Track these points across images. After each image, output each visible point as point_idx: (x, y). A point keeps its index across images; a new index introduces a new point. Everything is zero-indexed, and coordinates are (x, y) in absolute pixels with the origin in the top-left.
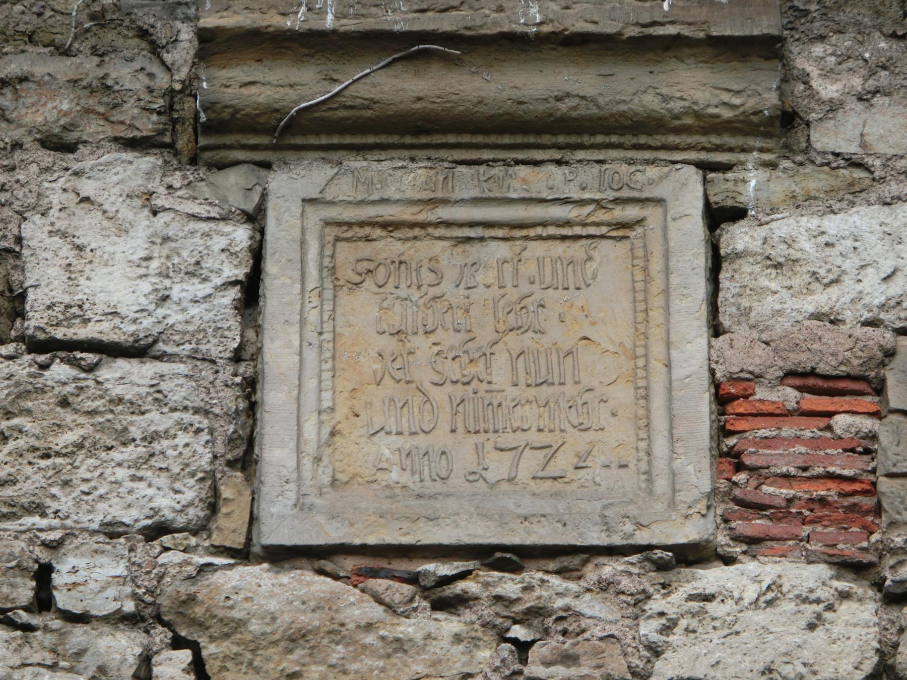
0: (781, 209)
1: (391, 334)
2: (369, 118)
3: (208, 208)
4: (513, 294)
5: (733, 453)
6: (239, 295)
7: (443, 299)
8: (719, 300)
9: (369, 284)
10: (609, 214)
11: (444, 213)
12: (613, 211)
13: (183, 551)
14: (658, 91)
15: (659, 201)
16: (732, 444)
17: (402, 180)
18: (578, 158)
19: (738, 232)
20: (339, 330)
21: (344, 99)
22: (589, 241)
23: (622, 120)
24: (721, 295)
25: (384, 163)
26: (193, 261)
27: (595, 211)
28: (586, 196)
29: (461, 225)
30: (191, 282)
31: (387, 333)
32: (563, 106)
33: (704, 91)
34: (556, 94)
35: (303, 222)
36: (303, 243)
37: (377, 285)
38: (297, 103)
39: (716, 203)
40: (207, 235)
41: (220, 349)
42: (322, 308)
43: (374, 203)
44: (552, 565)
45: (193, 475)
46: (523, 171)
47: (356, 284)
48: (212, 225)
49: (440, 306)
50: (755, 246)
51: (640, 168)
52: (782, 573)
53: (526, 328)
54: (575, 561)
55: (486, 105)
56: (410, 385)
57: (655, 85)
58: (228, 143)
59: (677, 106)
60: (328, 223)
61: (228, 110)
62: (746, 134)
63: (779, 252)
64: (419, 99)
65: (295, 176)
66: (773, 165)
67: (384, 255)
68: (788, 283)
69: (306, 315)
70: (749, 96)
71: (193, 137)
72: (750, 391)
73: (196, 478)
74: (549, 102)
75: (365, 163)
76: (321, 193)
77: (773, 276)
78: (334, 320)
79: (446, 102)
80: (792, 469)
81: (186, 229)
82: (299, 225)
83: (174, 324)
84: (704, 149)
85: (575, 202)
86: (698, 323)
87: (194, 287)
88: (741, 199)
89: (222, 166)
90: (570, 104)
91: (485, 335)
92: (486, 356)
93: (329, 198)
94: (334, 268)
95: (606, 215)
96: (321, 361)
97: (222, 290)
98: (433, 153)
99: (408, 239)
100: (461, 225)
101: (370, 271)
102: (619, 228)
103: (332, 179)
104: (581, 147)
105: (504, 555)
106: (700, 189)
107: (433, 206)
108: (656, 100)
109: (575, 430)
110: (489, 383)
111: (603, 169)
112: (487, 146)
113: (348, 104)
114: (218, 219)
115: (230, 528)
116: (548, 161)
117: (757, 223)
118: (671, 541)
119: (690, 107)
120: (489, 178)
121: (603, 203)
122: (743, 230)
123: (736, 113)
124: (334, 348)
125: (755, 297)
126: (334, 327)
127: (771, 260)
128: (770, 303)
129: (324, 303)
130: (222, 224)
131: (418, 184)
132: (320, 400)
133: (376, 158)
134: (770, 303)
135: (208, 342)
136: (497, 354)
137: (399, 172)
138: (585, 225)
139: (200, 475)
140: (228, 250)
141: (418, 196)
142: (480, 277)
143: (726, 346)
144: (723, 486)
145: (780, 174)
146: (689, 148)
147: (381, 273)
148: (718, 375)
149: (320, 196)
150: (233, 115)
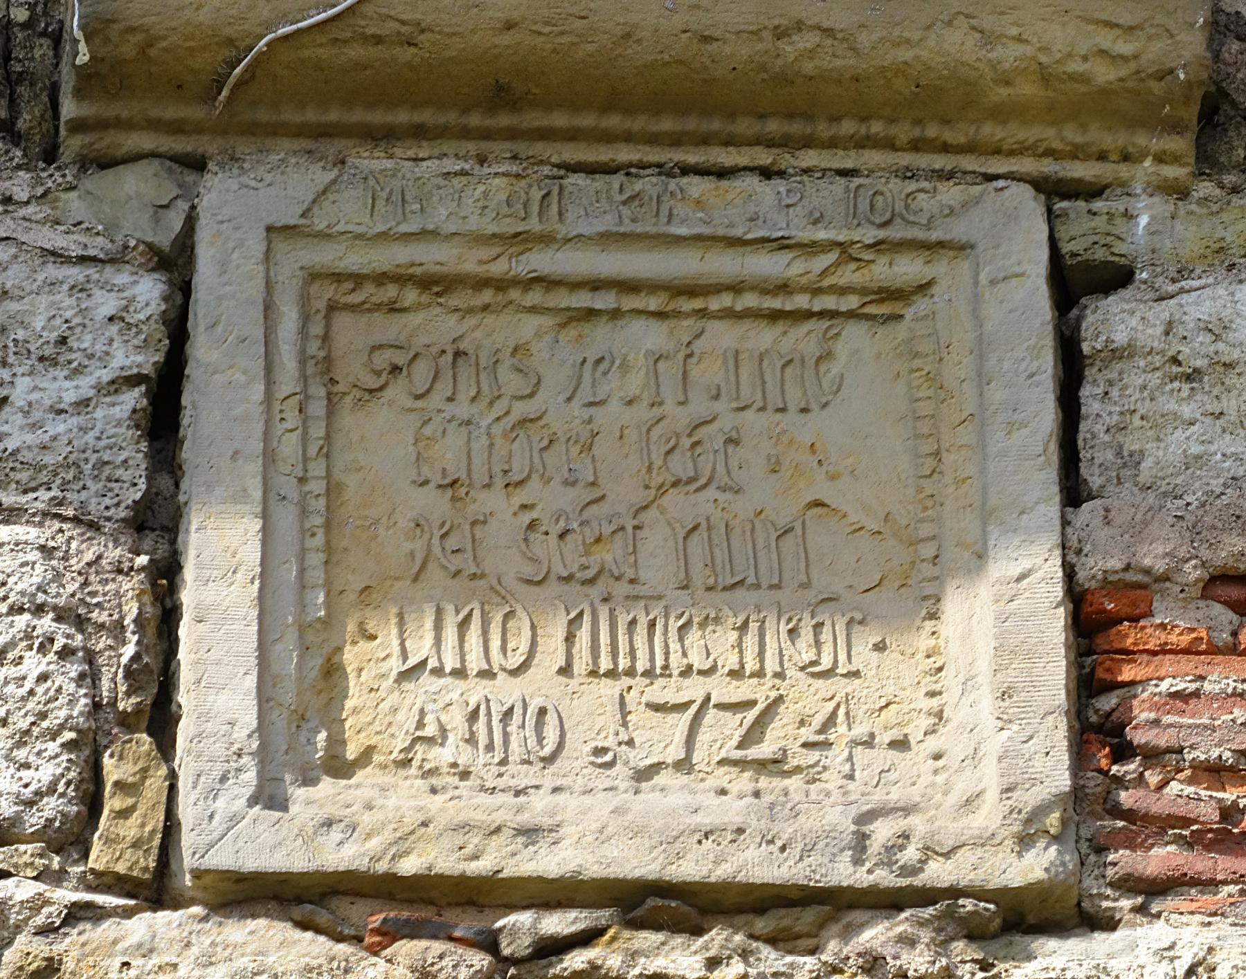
0: (1198, 271)
1: (440, 486)
2: (409, 65)
3: (82, 238)
4: (679, 418)
5: (1108, 725)
6: (145, 401)
7: (542, 423)
8: (1081, 437)
9: (397, 392)
10: (865, 271)
11: (540, 261)
12: (873, 267)
13: (35, 878)
14: (974, 22)
15: (963, 248)
16: (1107, 708)
17: (458, 201)
18: (804, 165)
19: (1115, 309)
20: (338, 475)
21: (363, 23)
22: (825, 324)
23: (899, 83)
24: (1083, 427)
25: (425, 164)
26: (54, 335)
27: (837, 264)
28: (822, 235)
29: (575, 285)
30: (50, 375)
31: (432, 485)
32: (788, 49)
33: (1064, 24)
34: (776, 22)
35: (268, 270)
36: (269, 308)
37: (410, 394)
38: (269, 27)
39: (1074, 255)
40: (79, 289)
41: (107, 501)
42: (305, 433)
43: (407, 237)
44: (762, 925)
45: (54, 734)
46: (697, 186)
47: (371, 391)
48: (92, 271)
49: (538, 437)
50: (1151, 336)
51: (925, 184)
52: (1216, 943)
53: (703, 481)
54: (809, 916)
55: (639, 41)
56: (476, 583)
57: (970, 10)
58: (124, 114)
59: (1008, 54)
60: (314, 275)
61: (139, 38)
62: (1134, 124)
63: (1196, 352)
64: (509, 26)
65: (253, 183)
66: (1180, 192)
67: (423, 340)
68: (1215, 407)
69: (275, 444)
70: (1150, 38)
71: (50, 113)
72: (1143, 608)
73: (59, 741)
74: (761, 40)
75: (389, 164)
76: (303, 215)
77: (1185, 394)
78: (327, 456)
79: (562, 33)
80: (1228, 754)
81: (41, 277)
82: (262, 275)
83: (18, 450)
84: (1050, 153)
85: (800, 245)
86: (1042, 476)
87: (56, 385)
88: (1120, 248)
89: (106, 163)
90: (801, 45)
91: (624, 492)
92: (631, 530)
93: (320, 225)
94: (328, 359)
95: (858, 274)
96: (303, 531)
97: (109, 394)
98: (523, 148)
99: (471, 311)
100: (575, 285)
101: (396, 369)
102: (882, 301)
103: (324, 192)
104: (809, 143)
105: (666, 902)
106: (1045, 228)
107: (521, 248)
108: (970, 42)
109: (801, 675)
110: (632, 581)
111: (853, 186)
112: (628, 138)
113: (371, 31)
114: (101, 261)
115: (117, 845)
116: (745, 169)
117: (1152, 295)
118: (995, 883)
119: (1033, 58)
120: (632, 198)
121: (853, 251)
122: (1126, 307)
123: (1123, 72)
124: (328, 508)
125: (1150, 433)
126: (328, 467)
127: (1180, 364)
128: (1179, 443)
129: (309, 424)
130: (109, 269)
131: (492, 204)
132: (302, 605)
133: (411, 153)
134: (1179, 443)
135: (84, 488)
136: (646, 529)
137: (455, 181)
138: (817, 291)
139: (69, 735)
140: (122, 319)
141: (492, 228)
142: (612, 385)
143: (1097, 521)
144: (1092, 784)
145: (1194, 207)
146: (1020, 151)
147: (422, 372)
148: (1081, 576)
149: (302, 221)
150: (143, 49)
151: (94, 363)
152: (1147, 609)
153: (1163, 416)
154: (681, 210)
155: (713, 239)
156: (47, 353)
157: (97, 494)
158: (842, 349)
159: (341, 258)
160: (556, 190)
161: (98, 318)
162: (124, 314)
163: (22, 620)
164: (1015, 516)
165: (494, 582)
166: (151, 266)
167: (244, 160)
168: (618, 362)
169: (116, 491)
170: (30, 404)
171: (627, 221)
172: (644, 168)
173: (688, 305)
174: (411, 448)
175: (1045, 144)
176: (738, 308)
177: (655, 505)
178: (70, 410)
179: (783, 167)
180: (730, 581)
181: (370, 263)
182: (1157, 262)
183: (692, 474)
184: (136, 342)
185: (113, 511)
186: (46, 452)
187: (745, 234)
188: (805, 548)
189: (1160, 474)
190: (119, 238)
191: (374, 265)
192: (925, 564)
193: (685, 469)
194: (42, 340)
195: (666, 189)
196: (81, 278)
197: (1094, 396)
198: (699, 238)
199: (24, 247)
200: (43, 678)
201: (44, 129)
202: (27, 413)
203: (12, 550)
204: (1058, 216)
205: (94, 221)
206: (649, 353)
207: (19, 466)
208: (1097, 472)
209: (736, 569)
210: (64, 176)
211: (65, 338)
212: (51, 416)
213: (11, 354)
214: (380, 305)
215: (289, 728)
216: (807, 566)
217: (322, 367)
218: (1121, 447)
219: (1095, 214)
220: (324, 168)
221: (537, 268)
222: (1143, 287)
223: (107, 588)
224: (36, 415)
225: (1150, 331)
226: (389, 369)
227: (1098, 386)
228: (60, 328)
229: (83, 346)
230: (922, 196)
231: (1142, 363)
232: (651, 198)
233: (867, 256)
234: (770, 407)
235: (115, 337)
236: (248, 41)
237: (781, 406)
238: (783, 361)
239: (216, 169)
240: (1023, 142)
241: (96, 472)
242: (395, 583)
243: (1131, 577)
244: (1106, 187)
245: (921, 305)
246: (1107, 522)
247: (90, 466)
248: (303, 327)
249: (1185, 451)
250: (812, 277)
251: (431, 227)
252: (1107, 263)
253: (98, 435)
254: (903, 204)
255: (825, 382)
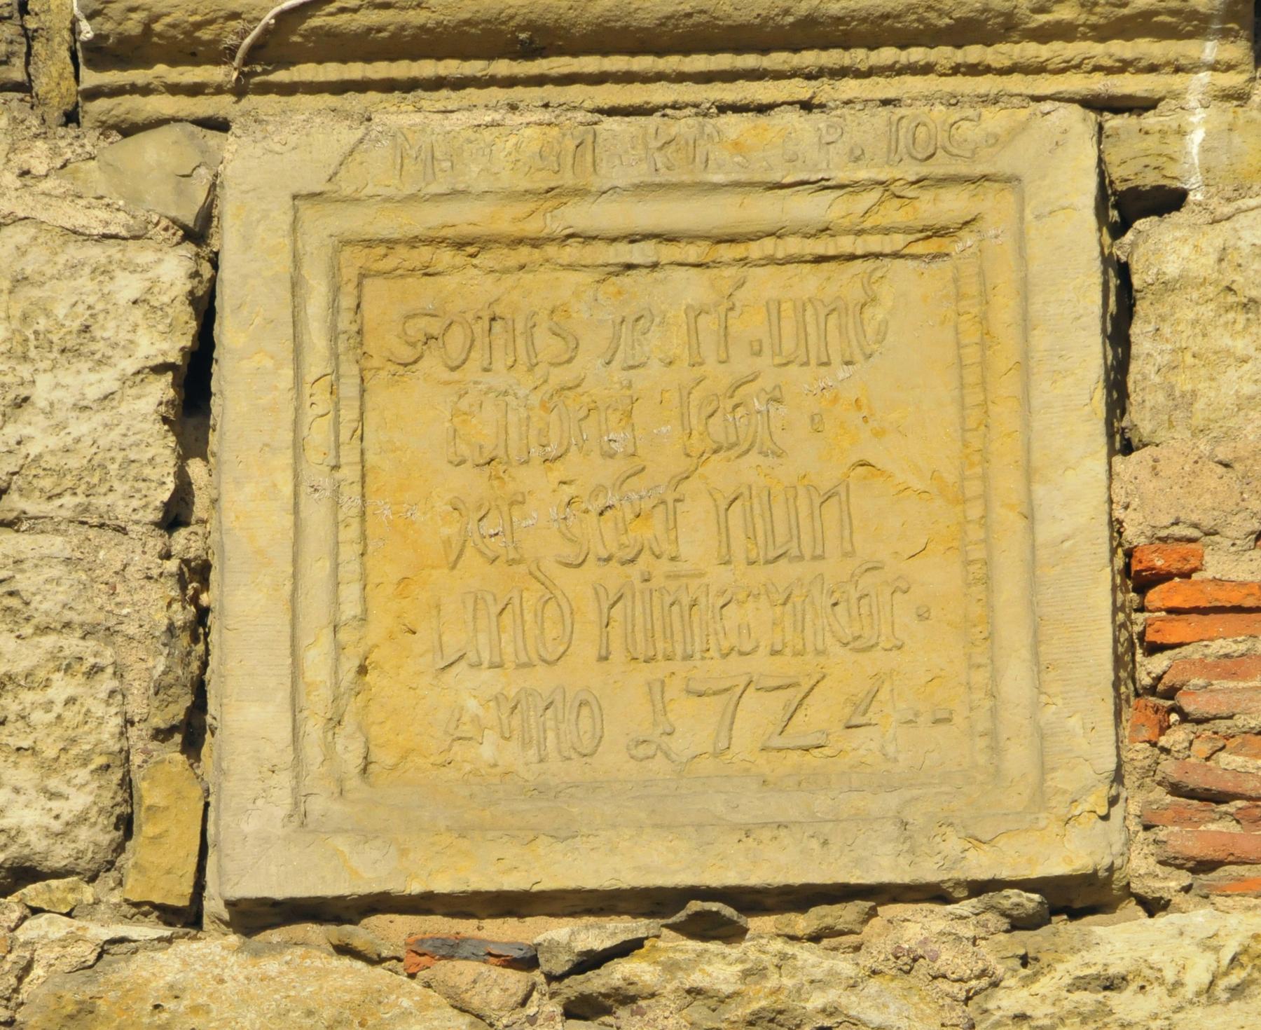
2: (422, 28)
3: (104, 215)
5: (1160, 687)
7: (580, 390)
9: (431, 364)
10: (909, 208)
12: (916, 203)
15: (1011, 180)
18: (845, 97)
25: (454, 116)
26: (76, 325)
27: (880, 202)
28: (862, 174)
30: (74, 368)
35: (295, 242)
36: (296, 285)
37: (447, 366)
41: (135, 503)
42: (337, 416)
51: (970, 113)
53: (745, 446)
69: (306, 432)
72: (1193, 563)
75: (418, 118)
77: (1239, 327)
81: (61, 259)
82: (288, 248)
83: (40, 456)
88: (1172, 170)
89: (128, 129)
92: (671, 505)
93: (347, 190)
99: (506, 271)
101: (429, 338)
107: (555, 202)
110: (673, 559)
112: (659, 77)
125: (1203, 372)
132: (336, 602)
133: (439, 106)
138: (860, 233)
141: (524, 184)
143: (1145, 474)
144: (1140, 757)
147: (456, 339)
149: (328, 187)
150: (147, 28)
151: (118, 353)
152: (1197, 564)
153: (1216, 353)
154: (717, 154)
155: (752, 184)
156: (69, 345)
157: (124, 496)
158: (886, 292)
159: (371, 223)
160: (590, 138)
161: (122, 302)
162: (148, 297)
163: (49, 641)
164: (1060, 472)
165: (533, 568)
166: (177, 238)
167: (267, 122)
168: (657, 320)
169: (144, 492)
170: (52, 405)
171: (663, 170)
172: (680, 109)
173: (727, 252)
174: (447, 425)
175: (1093, 62)
176: (780, 255)
177: (696, 474)
178: (95, 406)
179: (824, 100)
180: (772, 554)
181: (401, 227)
182: (1212, 182)
183: (733, 439)
184: (161, 327)
185: (141, 513)
186: (69, 454)
187: (784, 177)
188: (849, 514)
189: (1212, 417)
190: (140, 213)
191: (405, 228)
192: (971, 526)
193: (727, 434)
194: (64, 330)
195: (702, 132)
196: (103, 260)
197: (1145, 334)
198: (737, 184)
199: (44, 226)
200: (71, 701)
201: (63, 90)
202: (48, 414)
203: (36, 566)
204: (1108, 137)
205: (115, 196)
206: (689, 307)
207: (42, 473)
208: (1148, 416)
209: (778, 544)
210: (82, 146)
211: (87, 327)
212: (74, 414)
213: (32, 348)
214: (413, 270)
215: (325, 737)
216: (851, 533)
217: (353, 339)
218: (1172, 387)
219: (1147, 133)
220: (350, 127)
221: (571, 223)
222: (1197, 209)
223: (136, 597)
224: (59, 416)
225: (1203, 260)
226: (424, 339)
227: (1150, 323)
228: (83, 316)
229: (106, 335)
230: (967, 124)
231: (1195, 295)
232: (687, 143)
233: (910, 192)
234: (813, 362)
235: (140, 322)
236: (255, 14)
237: (825, 360)
238: (827, 311)
239: (239, 132)
240: (1068, 62)
241: (123, 472)
242: (433, 572)
243: (1179, 531)
244: (1161, 99)
245: (968, 239)
246: (1155, 472)
247: (116, 466)
248: (334, 301)
249: (1237, 391)
250: (855, 219)
251: (461, 187)
252: (1160, 188)
253: (124, 431)
254: (946, 135)
255: (870, 330)
